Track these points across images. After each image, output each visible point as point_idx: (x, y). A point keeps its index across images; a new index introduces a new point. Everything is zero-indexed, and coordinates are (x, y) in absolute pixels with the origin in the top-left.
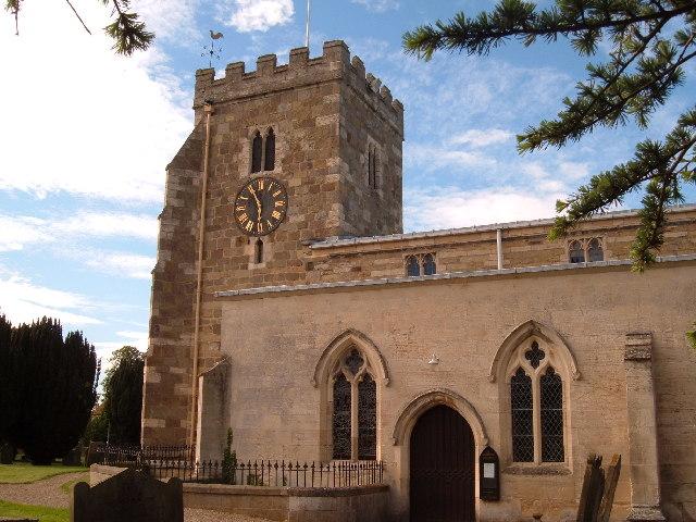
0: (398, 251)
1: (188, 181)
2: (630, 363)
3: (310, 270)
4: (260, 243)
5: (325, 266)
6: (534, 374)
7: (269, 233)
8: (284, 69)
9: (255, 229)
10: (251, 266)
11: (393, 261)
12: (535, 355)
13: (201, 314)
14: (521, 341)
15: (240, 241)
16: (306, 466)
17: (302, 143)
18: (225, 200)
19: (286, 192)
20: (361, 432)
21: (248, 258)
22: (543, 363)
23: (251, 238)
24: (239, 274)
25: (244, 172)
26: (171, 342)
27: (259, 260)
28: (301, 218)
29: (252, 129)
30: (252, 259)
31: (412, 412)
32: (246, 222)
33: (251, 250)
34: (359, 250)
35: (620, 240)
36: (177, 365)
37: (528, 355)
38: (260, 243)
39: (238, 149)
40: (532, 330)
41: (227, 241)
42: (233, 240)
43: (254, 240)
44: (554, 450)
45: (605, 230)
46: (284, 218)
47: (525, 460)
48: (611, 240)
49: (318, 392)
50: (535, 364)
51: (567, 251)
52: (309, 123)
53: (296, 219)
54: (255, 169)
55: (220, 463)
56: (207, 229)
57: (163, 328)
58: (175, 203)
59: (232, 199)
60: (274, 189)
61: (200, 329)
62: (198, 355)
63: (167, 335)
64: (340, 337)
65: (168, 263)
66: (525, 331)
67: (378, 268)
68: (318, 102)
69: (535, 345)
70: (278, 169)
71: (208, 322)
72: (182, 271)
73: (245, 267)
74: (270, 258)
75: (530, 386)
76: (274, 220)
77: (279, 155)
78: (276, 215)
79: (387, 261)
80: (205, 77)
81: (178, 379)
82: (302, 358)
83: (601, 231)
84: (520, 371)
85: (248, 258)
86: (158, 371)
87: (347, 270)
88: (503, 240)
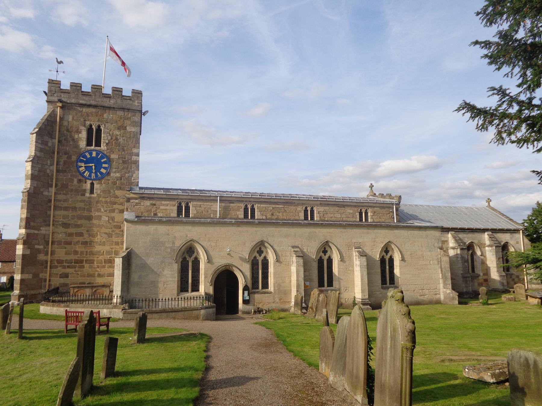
0: (174, 199)
1: (45, 143)
2: (297, 257)
3: (128, 202)
4: (92, 184)
5: (137, 201)
6: (260, 259)
7: (97, 179)
8: (107, 96)
9: (90, 176)
10: (87, 195)
11: (171, 203)
12: (260, 252)
13: (54, 216)
14: (257, 247)
15: (80, 181)
16: (197, 298)
17: (119, 137)
18: (69, 157)
19: (109, 161)
20: (193, 280)
21: (85, 191)
22: (263, 255)
23: (88, 181)
24: (80, 198)
25: (83, 144)
26: (36, 232)
27: (92, 192)
28: (118, 175)
29: (88, 123)
30: (88, 191)
31: (217, 273)
32: (84, 172)
33: (88, 186)
34: (155, 196)
35: (262, 206)
36: (39, 244)
37: (258, 252)
38: (92, 184)
39: (79, 132)
40: (262, 243)
41: (72, 181)
42: (75, 180)
43: (89, 182)
44: (265, 285)
45: (258, 202)
46: (108, 174)
47: (256, 289)
48: (259, 205)
49: (177, 264)
50: (260, 255)
51: (243, 208)
52: (122, 128)
53: (115, 175)
54: (89, 143)
55: (119, 296)
56: (58, 171)
57: (32, 224)
58: (38, 154)
59: (74, 158)
60: (102, 158)
61: (53, 225)
62: (52, 238)
63: (34, 228)
64: (189, 242)
65: (35, 187)
66: (259, 244)
67: (164, 205)
68: (128, 119)
69: (260, 248)
70: (103, 147)
71: (58, 222)
72: (42, 192)
73: (84, 195)
74: (99, 192)
75: (258, 263)
76: (101, 173)
77: (84, 135)
78: (103, 171)
79: (168, 202)
80: (54, 84)
81: (39, 251)
82: (169, 250)
83: (256, 202)
84: (255, 257)
85: (85, 191)
86: (29, 248)
87: (148, 204)
88: (220, 200)
